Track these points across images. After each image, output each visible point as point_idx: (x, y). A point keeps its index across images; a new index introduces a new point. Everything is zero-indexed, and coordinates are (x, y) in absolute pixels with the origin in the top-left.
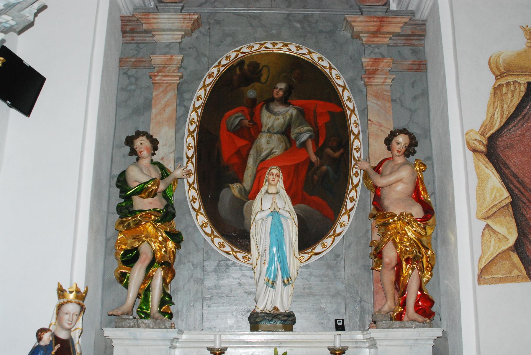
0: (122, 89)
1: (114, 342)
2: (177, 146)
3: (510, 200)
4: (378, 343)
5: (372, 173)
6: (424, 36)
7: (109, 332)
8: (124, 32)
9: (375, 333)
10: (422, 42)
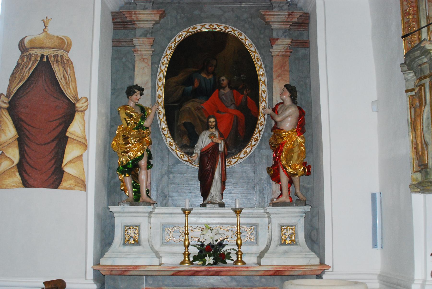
1: (115, 215)
3: (18, 136)
4: (272, 215)
6: (308, 24)
7: (113, 209)
9: (271, 209)
10: (307, 27)
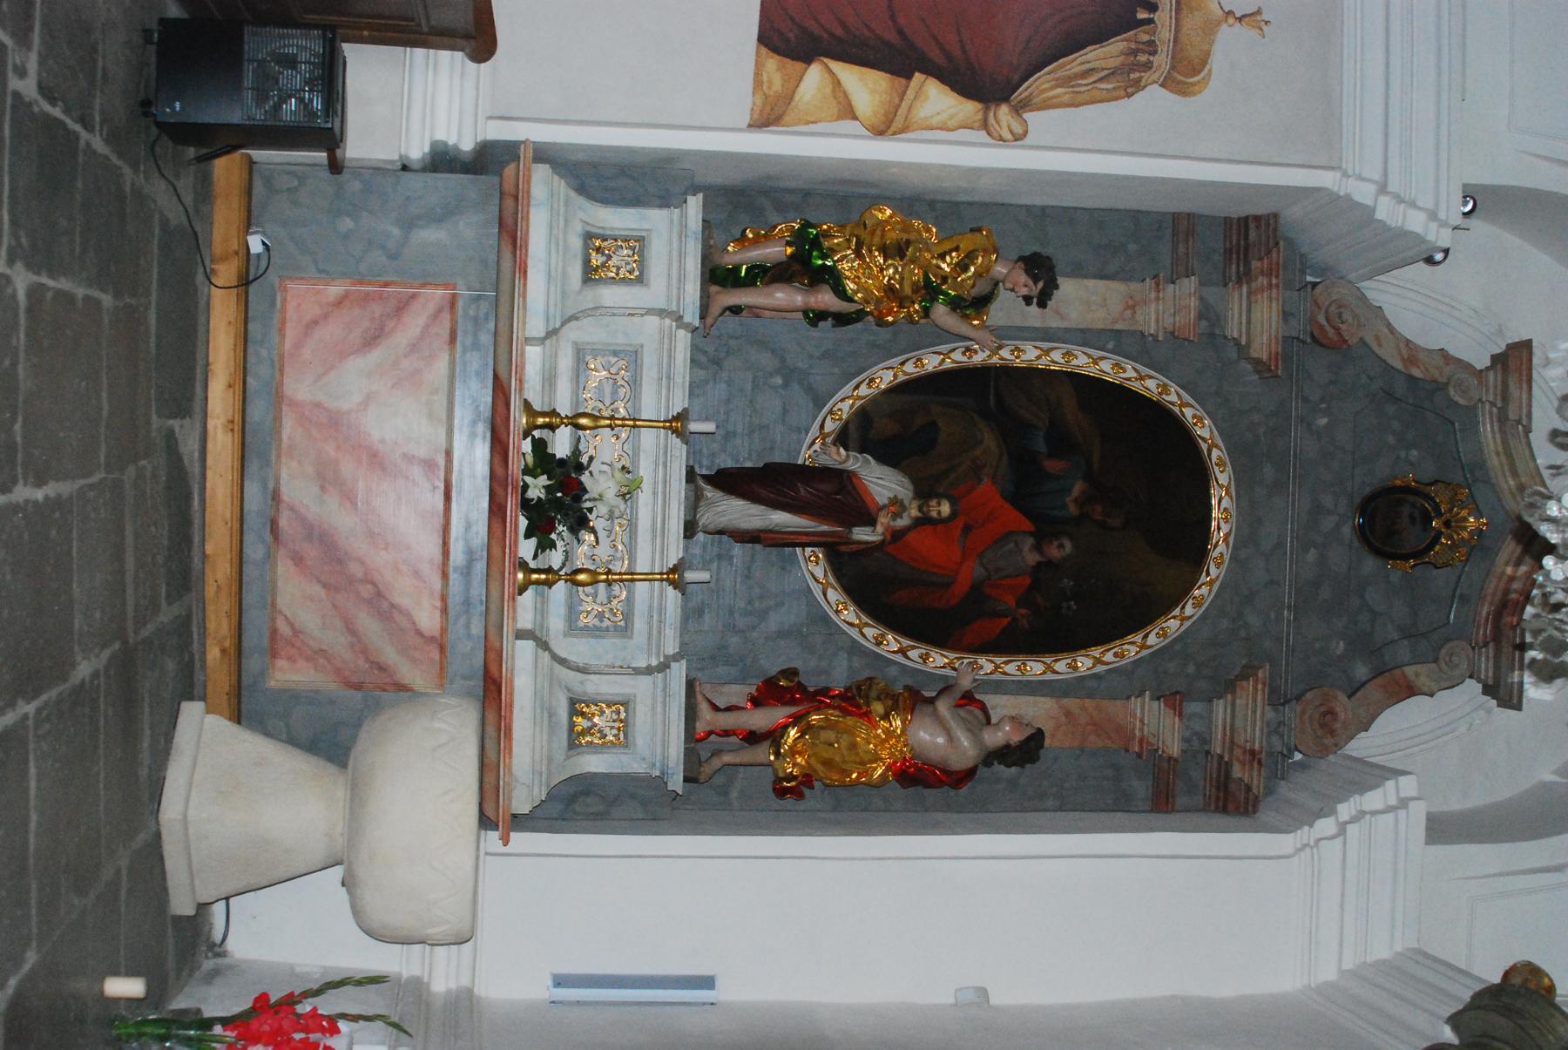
0: (1136, 215)
2: (1025, 337)
5: (958, 694)
7: (695, 204)
8: (1244, 222)
9: (679, 672)
